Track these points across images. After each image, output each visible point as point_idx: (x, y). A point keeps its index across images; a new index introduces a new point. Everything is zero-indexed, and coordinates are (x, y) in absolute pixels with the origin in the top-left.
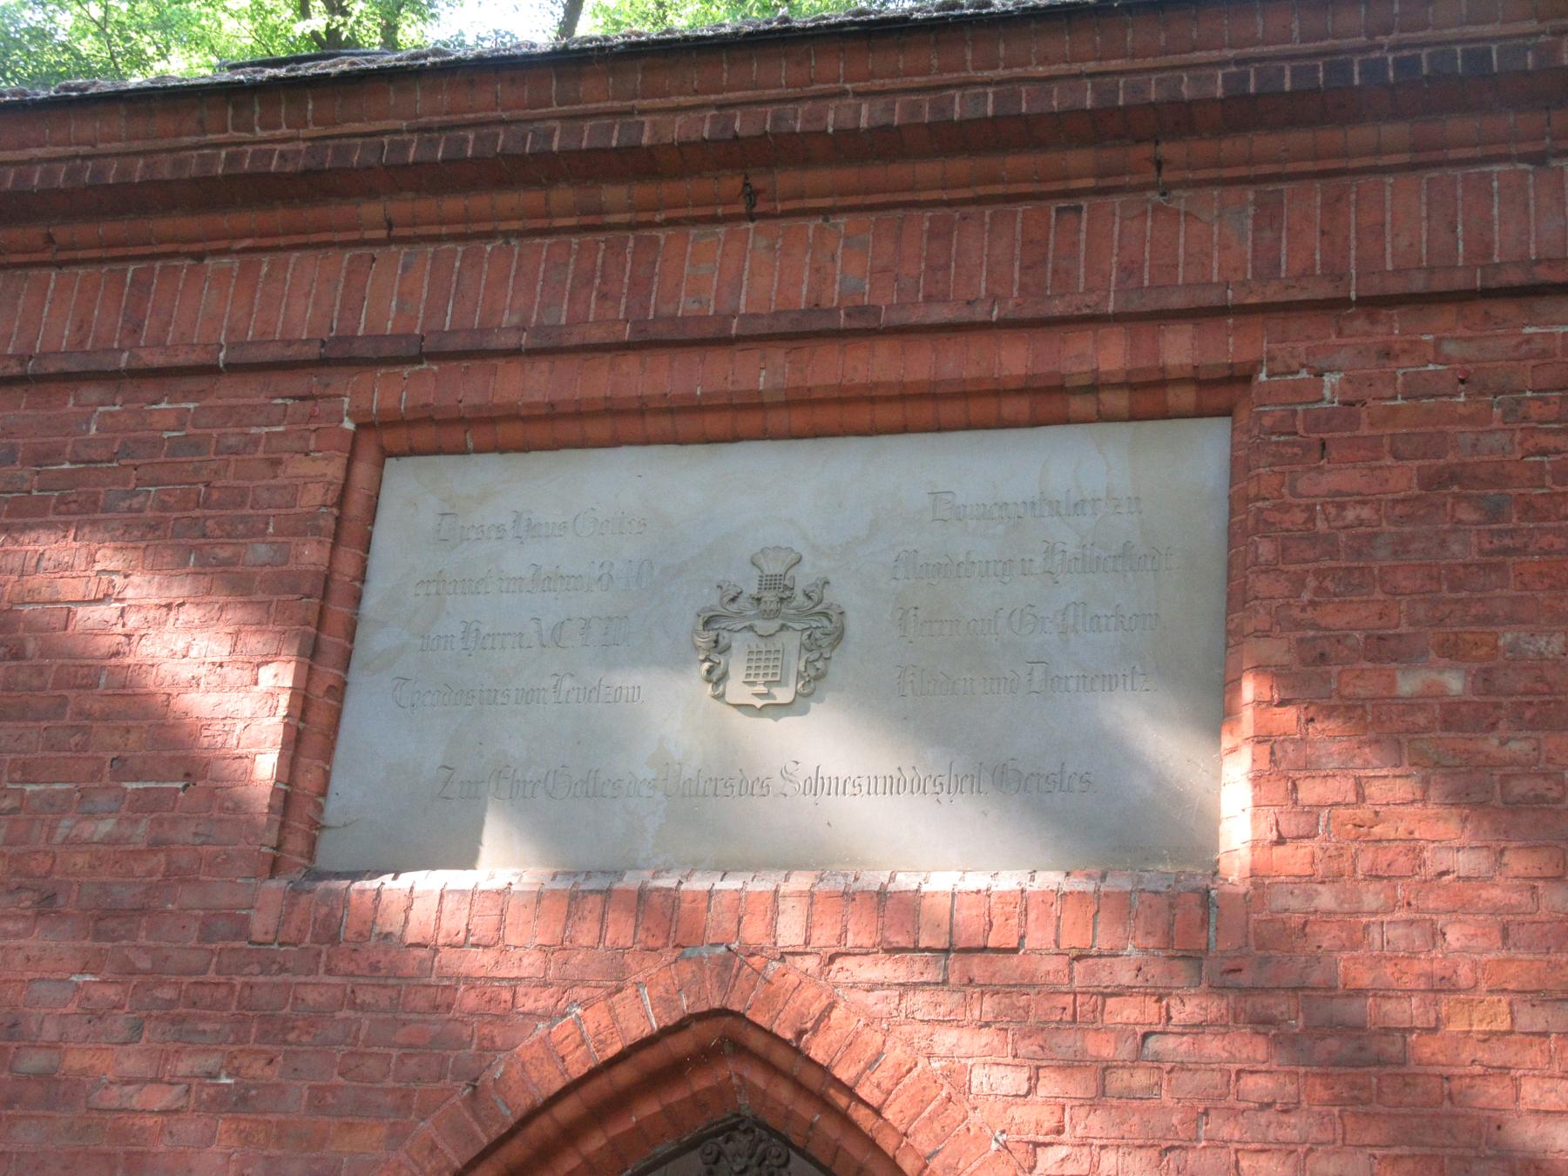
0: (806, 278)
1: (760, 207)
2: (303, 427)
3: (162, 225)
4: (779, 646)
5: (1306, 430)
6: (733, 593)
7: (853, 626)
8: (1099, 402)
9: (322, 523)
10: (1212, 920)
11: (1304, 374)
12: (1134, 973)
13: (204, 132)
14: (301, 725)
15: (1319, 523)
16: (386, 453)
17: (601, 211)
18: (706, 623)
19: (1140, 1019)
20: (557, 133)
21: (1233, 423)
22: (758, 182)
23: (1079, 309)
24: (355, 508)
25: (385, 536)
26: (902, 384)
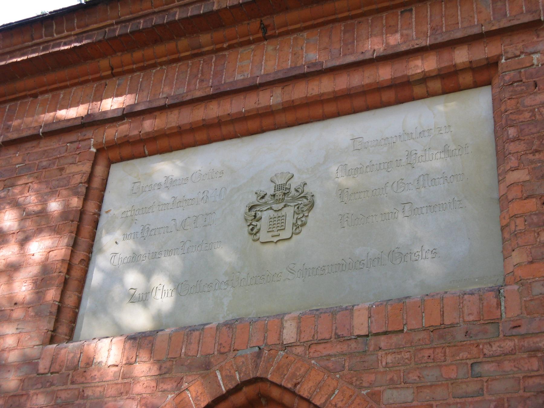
0: (290, 58)
1: (269, 33)
2: (74, 153)
3: (20, 84)
4: (284, 214)
5: (527, 79)
6: (262, 194)
7: (318, 202)
8: (427, 87)
9: (80, 190)
10: (503, 304)
11: (523, 56)
12: (463, 335)
13: (33, 39)
14: (67, 276)
15: (537, 117)
16: (110, 162)
17: (200, 47)
18: (250, 209)
19: (469, 356)
20: (178, 13)
21: (492, 86)
22: (267, 21)
23: (413, 46)
24: (96, 183)
25: (110, 197)
26: (334, 92)
